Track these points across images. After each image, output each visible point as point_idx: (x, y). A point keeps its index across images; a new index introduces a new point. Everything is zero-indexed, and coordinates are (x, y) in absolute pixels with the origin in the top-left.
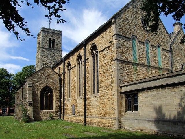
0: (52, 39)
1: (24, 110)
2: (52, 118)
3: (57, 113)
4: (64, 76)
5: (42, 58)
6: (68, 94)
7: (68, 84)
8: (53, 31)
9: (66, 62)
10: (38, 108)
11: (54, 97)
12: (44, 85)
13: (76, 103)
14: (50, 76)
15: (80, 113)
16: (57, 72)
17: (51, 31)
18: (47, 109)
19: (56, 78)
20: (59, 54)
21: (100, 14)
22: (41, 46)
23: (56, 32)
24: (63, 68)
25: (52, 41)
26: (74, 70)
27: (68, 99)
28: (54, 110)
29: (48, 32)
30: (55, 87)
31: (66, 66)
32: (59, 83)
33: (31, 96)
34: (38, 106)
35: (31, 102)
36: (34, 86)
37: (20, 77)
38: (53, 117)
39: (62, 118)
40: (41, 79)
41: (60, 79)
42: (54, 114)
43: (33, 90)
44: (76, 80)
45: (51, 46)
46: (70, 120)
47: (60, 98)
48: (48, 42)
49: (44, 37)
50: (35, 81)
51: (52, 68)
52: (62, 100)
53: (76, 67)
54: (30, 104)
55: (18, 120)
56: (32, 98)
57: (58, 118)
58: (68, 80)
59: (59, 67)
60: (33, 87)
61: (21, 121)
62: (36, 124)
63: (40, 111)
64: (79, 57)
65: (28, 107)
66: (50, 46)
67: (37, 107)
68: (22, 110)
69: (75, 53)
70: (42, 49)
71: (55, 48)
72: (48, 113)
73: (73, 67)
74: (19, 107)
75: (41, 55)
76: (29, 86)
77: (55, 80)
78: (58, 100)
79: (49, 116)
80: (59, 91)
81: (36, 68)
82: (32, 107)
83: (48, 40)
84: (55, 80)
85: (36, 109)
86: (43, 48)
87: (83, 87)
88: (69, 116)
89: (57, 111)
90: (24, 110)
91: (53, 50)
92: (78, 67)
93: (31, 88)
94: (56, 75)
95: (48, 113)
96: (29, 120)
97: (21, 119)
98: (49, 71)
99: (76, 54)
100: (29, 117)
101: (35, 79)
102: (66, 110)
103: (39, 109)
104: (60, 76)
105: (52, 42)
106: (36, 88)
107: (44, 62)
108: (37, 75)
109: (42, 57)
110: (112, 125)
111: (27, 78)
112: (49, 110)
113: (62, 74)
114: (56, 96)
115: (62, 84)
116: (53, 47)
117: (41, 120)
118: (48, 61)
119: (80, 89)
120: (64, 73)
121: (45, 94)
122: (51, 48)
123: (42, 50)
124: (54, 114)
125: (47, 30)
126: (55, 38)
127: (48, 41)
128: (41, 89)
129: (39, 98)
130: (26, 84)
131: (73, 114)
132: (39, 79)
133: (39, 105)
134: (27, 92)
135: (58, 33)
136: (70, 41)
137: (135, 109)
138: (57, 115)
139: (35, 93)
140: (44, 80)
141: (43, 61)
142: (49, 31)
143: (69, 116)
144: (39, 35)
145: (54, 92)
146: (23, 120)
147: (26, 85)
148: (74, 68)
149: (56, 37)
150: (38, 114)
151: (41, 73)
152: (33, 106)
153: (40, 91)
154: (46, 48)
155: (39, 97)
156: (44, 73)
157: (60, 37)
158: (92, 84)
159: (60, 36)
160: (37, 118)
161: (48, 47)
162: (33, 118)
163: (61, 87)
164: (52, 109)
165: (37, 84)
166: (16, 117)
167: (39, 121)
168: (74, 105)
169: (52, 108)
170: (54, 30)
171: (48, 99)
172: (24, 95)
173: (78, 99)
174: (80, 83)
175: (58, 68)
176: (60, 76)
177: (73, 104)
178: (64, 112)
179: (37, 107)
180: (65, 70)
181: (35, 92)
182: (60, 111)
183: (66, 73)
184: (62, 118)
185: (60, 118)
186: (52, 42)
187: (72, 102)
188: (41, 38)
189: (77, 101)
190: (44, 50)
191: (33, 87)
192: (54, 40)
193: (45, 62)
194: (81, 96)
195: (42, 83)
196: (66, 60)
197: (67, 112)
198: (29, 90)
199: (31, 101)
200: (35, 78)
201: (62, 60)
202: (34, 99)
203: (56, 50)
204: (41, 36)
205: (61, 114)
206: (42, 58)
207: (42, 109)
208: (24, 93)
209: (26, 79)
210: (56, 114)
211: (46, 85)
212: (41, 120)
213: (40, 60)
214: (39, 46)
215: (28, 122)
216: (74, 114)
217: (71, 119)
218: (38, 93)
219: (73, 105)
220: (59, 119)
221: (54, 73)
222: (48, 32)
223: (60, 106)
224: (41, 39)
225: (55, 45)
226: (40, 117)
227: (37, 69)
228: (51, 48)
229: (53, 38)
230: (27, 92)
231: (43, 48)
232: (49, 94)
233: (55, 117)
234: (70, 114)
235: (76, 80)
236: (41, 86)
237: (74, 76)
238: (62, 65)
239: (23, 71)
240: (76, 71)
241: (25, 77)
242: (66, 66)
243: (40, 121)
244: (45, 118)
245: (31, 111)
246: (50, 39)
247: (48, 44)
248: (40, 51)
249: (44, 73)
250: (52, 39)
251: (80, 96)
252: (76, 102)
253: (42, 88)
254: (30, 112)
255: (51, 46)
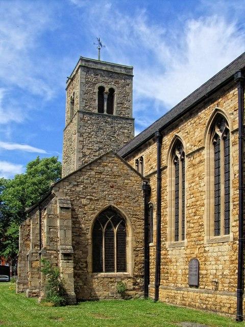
0: (107, 90)
1: (51, 272)
2: (124, 295)
3: (138, 281)
4: (160, 179)
5: (81, 139)
6: (173, 229)
7: (173, 202)
8: (109, 68)
9: (168, 140)
10: (86, 267)
11: (129, 238)
12: (102, 205)
13: (205, 254)
14: (118, 180)
15: (217, 283)
16: (134, 167)
17: (104, 68)
18: (109, 269)
19: (136, 185)
20: (125, 128)
21: (231, 29)
22: (77, 107)
23: (118, 70)
24: (156, 156)
25: (106, 93)
26: (198, 160)
27: (173, 242)
28: (130, 271)
29: (96, 71)
30: (131, 209)
31: (166, 152)
32: (142, 200)
33: (69, 234)
34: (86, 262)
35: (69, 251)
36: (76, 208)
37: (23, 189)
38: (127, 290)
39: (152, 296)
40: (94, 188)
41: (147, 191)
42: (129, 284)
43: (72, 217)
44: (205, 189)
45: (105, 108)
46: (178, 302)
47: (147, 240)
48: (96, 97)
49: (87, 83)
50: (78, 193)
51: (123, 157)
52: (150, 244)
53: (204, 152)
54: (66, 256)
55: (29, 296)
56: (70, 239)
57: (140, 293)
58: (174, 189)
59: (140, 155)
60: (73, 210)
61: (43, 300)
62: (86, 308)
63: (92, 276)
64: (219, 120)
65: (61, 263)
66: (101, 109)
67: (85, 265)
68: (45, 272)
69: (200, 110)
70: (81, 115)
71: (114, 114)
72: (112, 280)
73: (194, 152)
74: (31, 263)
75: (78, 132)
76: (61, 208)
77: (131, 192)
78: (141, 247)
79: (115, 287)
80: (143, 222)
81: (64, 165)
82: (71, 264)
83: (96, 90)
84: (131, 192)
85: (81, 269)
86: (84, 113)
87: (231, 207)
88: (179, 289)
89: (137, 276)
90: (51, 272)
91: (109, 117)
92: (212, 151)
93: (68, 214)
94: (134, 178)
95: (112, 280)
96: (64, 299)
97: (42, 294)
98: (114, 166)
99: (206, 115)
100: (62, 292)
101: (78, 189)
102: (167, 273)
103: (90, 269)
104: (147, 179)
105: (106, 96)
106: (79, 212)
107: (85, 150)
108: (82, 178)
109: (81, 135)
110: (218, 307)
111: (55, 184)
112: (115, 273)
113: (151, 175)
114: (135, 234)
115: (154, 200)
116: (110, 110)
117: (95, 299)
118: (96, 147)
119: (217, 213)
120: (160, 170)
121: (104, 230)
122: (105, 113)
123: (82, 119)
124: (129, 284)
125: (93, 66)
126: (114, 87)
127: (97, 94)
128: (94, 216)
129: (90, 241)
130: (53, 200)
131: (191, 286)
132: (89, 190)
133: (89, 259)
134: (58, 223)
135: (123, 72)
136: (150, 102)
137: (112, 272)
138: (137, 287)
139: (77, 225)
140: (104, 191)
141: (83, 146)
142: (99, 66)
143: (179, 289)
144: (72, 80)
145: (128, 224)
146: (48, 298)
147: (56, 205)
148: (196, 155)
149: (117, 83)
150: (87, 282)
151: (93, 173)
152: (74, 263)
153: (92, 222)
154: (91, 114)
155: (89, 236)
156: (101, 173)
157: (129, 85)
158: (173, 214)
159: (128, 81)
160: (83, 296)
161: (96, 111)
162: (73, 293)
163: (148, 209)
164: (125, 270)
165: (84, 201)
166: (22, 287)
167: (89, 300)
168: (195, 259)
169: (122, 267)
170: (113, 66)
171: (113, 244)
172: (49, 232)
173: (211, 242)
174: (217, 196)
175: (137, 157)
176: (147, 179)
177: (194, 256)
178: (158, 279)
179: (85, 265)
180: (164, 163)
181: (79, 223)
182: (146, 276)
183: (167, 171)
184: (152, 296)
185: (146, 295)
186: (106, 96)
187: (188, 251)
188: (78, 87)
189: (207, 249)
190: (87, 117)
191: (70, 209)
192: (112, 91)
193: (89, 149)
194: (222, 235)
195: (98, 200)
196: (167, 134)
197: (170, 278)
198: (63, 219)
199: (69, 248)
200: (77, 185)
201: (152, 136)
202: (76, 245)
203: (117, 117)
204: (77, 83)
205: (147, 282)
206: (81, 139)
207: (97, 268)
208: (50, 227)
209: (52, 188)
210: (135, 284)
211: (107, 204)
212: (95, 299)
213: (75, 145)
214: (72, 109)
215: (62, 304)
216: (197, 287)
217: (184, 300)
218: (87, 227)
219: (194, 263)
220: (142, 298)
221: (130, 172)
222: (96, 71)
223: (147, 263)
224: (77, 89)
225: (115, 106)
226: (92, 290)
227: (70, 166)
228: (105, 113)
229: (110, 86)
230: (58, 223)
231: (84, 113)
232: (115, 230)
233: (131, 290)
234: (179, 285)
235: (205, 189)
236: (93, 207)
237: (197, 178)
238: (153, 148)
239: (30, 174)
240: (206, 163)
241: (52, 183)
242: (166, 152)
243: (93, 300)
244: (106, 293)
245: (69, 274)
246: (101, 89)
247: (97, 102)
248: (75, 121)
249: (101, 173)
250: (107, 90)
251: (177, 239)
252: (205, 251)
253: (97, 212)
254: (66, 277)
255: (105, 108)
